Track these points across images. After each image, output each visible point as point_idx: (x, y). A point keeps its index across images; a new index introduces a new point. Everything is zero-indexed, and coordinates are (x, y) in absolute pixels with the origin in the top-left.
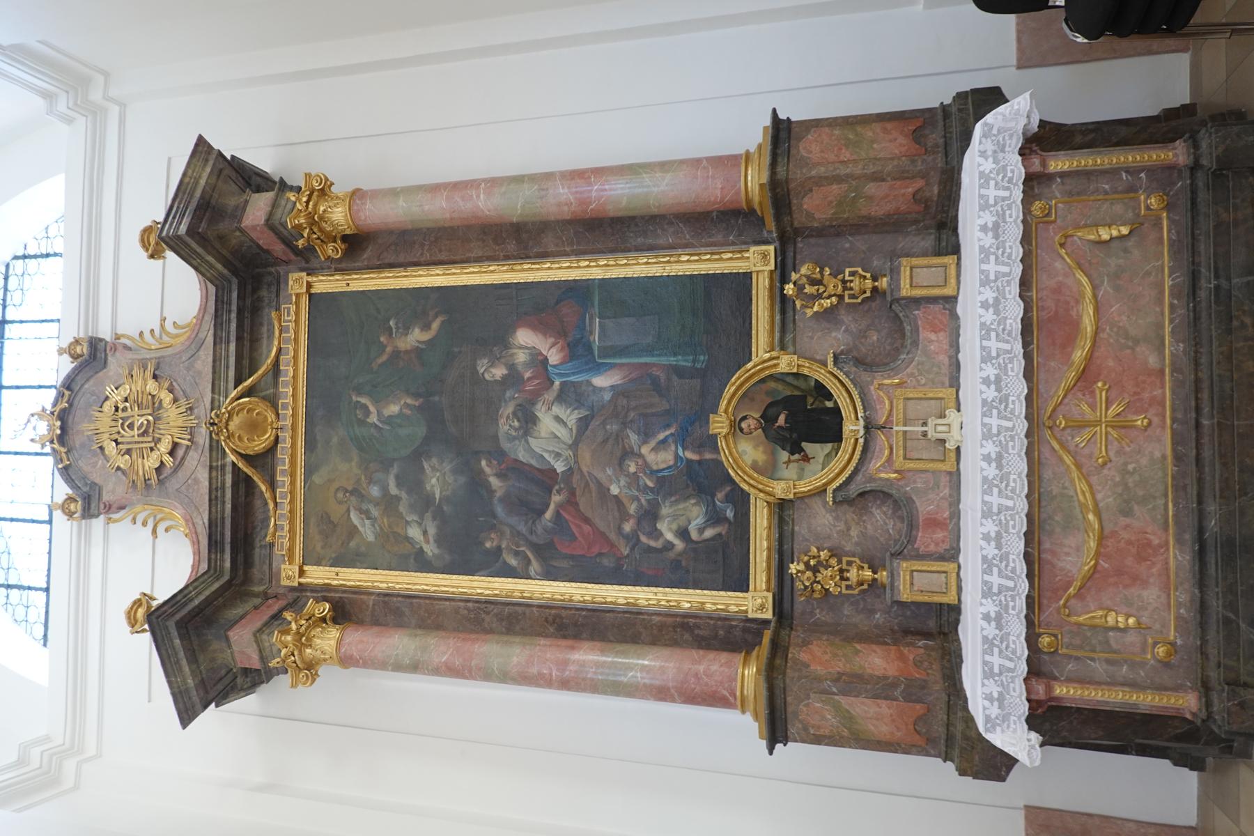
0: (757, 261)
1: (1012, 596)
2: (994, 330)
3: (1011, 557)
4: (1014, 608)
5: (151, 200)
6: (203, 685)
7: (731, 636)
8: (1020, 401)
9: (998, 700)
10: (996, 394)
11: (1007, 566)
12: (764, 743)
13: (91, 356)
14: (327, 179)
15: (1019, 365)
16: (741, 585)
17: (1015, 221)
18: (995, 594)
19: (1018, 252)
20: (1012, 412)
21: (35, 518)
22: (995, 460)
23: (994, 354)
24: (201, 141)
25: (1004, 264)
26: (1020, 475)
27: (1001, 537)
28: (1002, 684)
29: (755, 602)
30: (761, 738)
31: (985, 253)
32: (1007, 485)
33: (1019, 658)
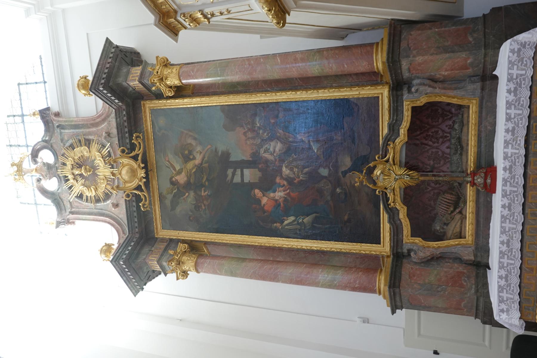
0: (384, 93)
1: (512, 302)
2: (509, 181)
3: (512, 285)
4: (524, 84)
5: (87, 66)
6: (136, 291)
7: (371, 264)
8: (526, 100)
9: (508, 207)
10: (507, 248)
11: (510, 289)
12: (389, 309)
13: (83, 185)
14: (168, 60)
15: (522, 160)
16: (376, 240)
17: (516, 275)
18: (513, 119)
19: (521, 181)
20: (514, 256)
21: (26, 132)
22: (508, 207)
23: (505, 299)
24: (107, 39)
25: (513, 224)
26: (520, 176)
27: (511, 206)
28: (508, 305)
29: (384, 248)
30: (388, 306)
31: (505, 181)
32: (513, 218)
33: (519, 223)
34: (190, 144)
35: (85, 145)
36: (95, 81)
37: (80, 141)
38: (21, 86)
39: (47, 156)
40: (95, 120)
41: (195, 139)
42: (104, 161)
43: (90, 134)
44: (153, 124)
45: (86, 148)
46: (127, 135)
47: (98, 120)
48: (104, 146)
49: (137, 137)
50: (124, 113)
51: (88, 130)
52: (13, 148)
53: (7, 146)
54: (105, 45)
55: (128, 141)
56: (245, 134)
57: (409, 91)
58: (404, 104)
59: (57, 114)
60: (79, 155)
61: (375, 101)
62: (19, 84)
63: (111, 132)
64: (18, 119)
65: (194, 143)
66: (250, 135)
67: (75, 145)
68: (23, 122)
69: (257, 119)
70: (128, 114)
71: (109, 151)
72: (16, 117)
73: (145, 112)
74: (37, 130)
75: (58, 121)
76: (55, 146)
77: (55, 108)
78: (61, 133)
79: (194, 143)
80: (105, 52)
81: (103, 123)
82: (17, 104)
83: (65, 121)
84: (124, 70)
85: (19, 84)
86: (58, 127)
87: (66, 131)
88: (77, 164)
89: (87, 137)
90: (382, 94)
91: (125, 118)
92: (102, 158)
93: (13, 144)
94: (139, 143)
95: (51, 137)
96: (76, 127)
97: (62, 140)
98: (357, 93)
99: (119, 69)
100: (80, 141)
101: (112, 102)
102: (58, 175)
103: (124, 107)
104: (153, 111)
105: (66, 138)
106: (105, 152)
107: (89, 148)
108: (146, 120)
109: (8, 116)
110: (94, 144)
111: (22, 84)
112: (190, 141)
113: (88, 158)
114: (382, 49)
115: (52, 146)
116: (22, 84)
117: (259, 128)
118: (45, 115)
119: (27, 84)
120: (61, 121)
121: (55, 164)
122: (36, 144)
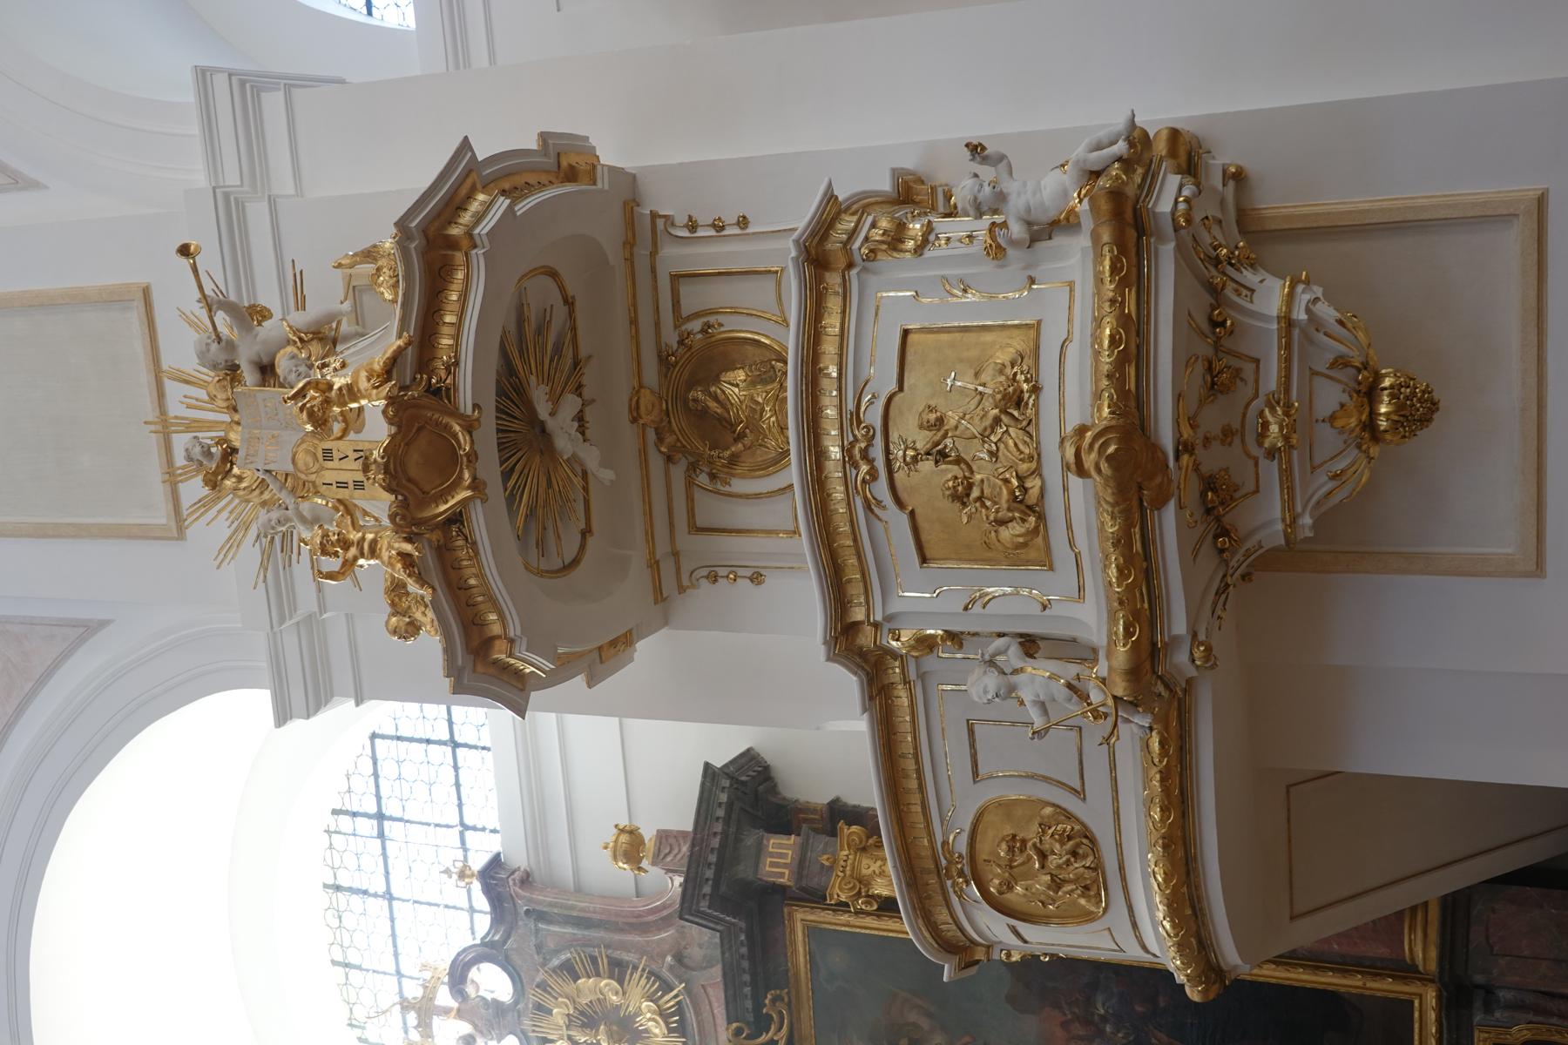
34: (915, 1025)
35: (611, 977)
36: (689, 892)
37: (594, 960)
38: (377, 741)
39: (493, 982)
40: (640, 916)
41: (929, 1015)
42: (667, 1024)
43: (623, 946)
44: (812, 962)
45: (614, 983)
46: (747, 990)
47: (651, 918)
48: (667, 988)
49: (774, 1001)
50: (743, 937)
51: (617, 937)
52: (342, 897)
53: (326, 886)
54: (703, 784)
55: (749, 1004)
56: (1065, 1025)
57: (1488, 1009)
58: (1476, 1034)
59: (526, 880)
60: (593, 997)
61: (1401, 1011)
62: (374, 736)
63: (686, 953)
64: (367, 826)
65: (925, 1024)
66: (1077, 1029)
67: (579, 968)
68: (381, 835)
69: (1100, 998)
70: (750, 937)
71: (678, 1003)
72: (359, 820)
73: (793, 931)
74: (470, 920)
75: (530, 900)
76: (515, 957)
77: (519, 859)
78: (537, 931)
79: (925, 1024)
80: (704, 806)
81: (659, 930)
82: (363, 784)
83: (550, 904)
84: (750, 840)
85: (374, 736)
86: (527, 912)
87: (556, 929)
88: (582, 1013)
89: (617, 954)
90: (1420, 996)
91: (744, 950)
92: (661, 1015)
93: (345, 884)
94: (780, 1013)
95: (507, 936)
96: (583, 922)
97: (539, 948)
98: (1360, 984)
99: (738, 840)
100: (594, 960)
101: (718, 921)
102: (523, 1032)
103: (743, 925)
104: (813, 932)
105: (551, 944)
106: (668, 1001)
107: (621, 982)
108: (795, 951)
109: (335, 812)
110: (636, 976)
111: (383, 737)
112: (913, 1017)
113: (618, 1007)
114: (1425, 935)
115: (507, 957)
116: (383, 737)
117: (1104, 1019)
118: (494, 877)
119: (399, 738)
120: (539, 902)
121: (516, 1002)
122: (465, 950)
